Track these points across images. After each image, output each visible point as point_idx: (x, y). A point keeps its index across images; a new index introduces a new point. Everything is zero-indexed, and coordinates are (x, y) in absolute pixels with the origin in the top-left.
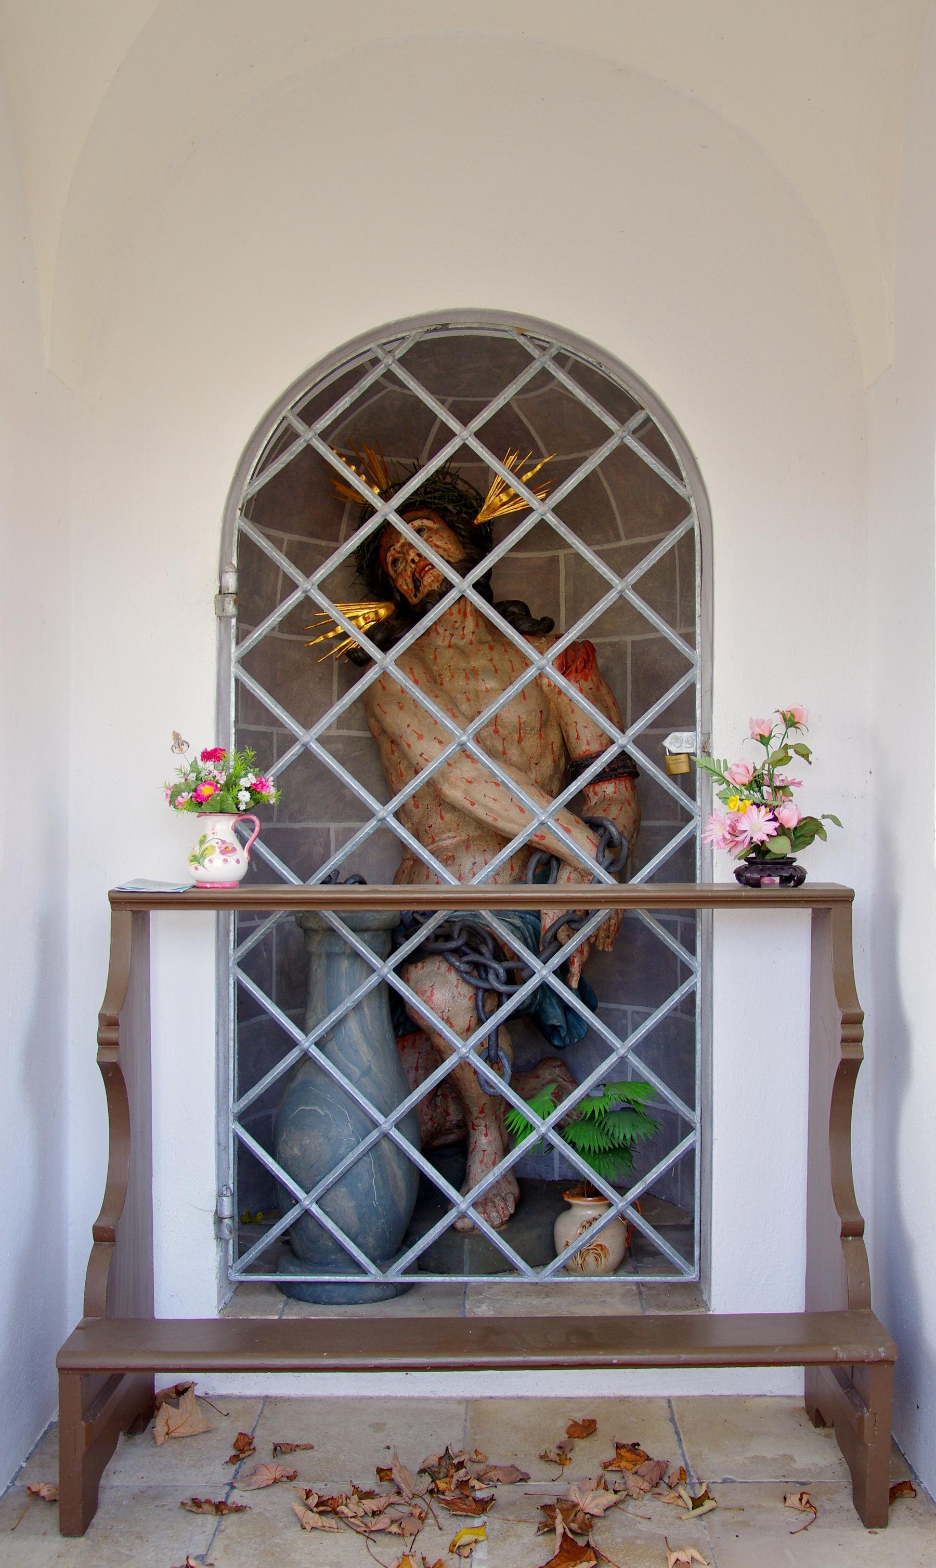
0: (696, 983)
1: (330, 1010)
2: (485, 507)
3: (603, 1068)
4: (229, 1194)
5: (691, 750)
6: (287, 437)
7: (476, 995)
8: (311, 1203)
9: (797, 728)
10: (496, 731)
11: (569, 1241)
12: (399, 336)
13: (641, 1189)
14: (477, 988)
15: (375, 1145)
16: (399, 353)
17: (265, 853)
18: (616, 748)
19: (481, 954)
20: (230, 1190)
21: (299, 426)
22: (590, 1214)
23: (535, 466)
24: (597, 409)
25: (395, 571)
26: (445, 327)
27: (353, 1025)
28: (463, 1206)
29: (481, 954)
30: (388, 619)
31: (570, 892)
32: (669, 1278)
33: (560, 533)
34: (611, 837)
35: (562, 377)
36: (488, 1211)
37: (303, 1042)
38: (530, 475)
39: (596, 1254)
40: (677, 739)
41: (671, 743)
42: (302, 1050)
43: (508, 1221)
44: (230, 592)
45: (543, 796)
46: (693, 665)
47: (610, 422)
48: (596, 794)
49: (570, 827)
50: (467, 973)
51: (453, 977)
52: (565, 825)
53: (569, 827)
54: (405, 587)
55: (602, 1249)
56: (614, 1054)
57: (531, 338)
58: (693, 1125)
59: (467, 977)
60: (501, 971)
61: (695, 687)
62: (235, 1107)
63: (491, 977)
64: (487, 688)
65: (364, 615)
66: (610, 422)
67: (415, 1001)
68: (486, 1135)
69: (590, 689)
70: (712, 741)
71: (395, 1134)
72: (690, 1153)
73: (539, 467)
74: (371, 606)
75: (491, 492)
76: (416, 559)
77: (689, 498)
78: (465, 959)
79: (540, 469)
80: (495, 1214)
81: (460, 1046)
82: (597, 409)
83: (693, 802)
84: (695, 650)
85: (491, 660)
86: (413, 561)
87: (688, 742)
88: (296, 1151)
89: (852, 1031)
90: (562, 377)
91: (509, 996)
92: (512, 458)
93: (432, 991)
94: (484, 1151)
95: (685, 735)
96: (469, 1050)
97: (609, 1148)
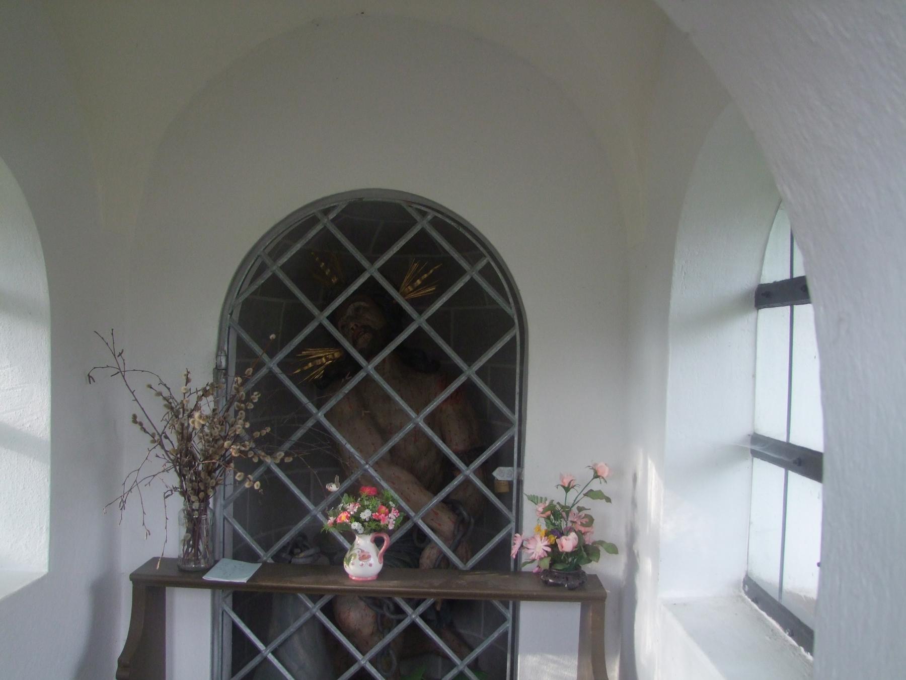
1: (282, 631)
5: (510, 479)
6: (262, 268)
9: (573, 487)
16: (331, 216)
21: (268, 261)
27: (296, 639)
30: (338, 359)
34: (464, 519)
37: (263, 652)
38: (426, 276)
47: (464, 264)
49: (438, 512)
63: (385, 608)
65: (325, 356)
74: (330, 350)
75: (403, 284)
76: (355, 328)
81: (360, 659)
82: (456, 255)
83: (510, 513)
86: (352, 328)
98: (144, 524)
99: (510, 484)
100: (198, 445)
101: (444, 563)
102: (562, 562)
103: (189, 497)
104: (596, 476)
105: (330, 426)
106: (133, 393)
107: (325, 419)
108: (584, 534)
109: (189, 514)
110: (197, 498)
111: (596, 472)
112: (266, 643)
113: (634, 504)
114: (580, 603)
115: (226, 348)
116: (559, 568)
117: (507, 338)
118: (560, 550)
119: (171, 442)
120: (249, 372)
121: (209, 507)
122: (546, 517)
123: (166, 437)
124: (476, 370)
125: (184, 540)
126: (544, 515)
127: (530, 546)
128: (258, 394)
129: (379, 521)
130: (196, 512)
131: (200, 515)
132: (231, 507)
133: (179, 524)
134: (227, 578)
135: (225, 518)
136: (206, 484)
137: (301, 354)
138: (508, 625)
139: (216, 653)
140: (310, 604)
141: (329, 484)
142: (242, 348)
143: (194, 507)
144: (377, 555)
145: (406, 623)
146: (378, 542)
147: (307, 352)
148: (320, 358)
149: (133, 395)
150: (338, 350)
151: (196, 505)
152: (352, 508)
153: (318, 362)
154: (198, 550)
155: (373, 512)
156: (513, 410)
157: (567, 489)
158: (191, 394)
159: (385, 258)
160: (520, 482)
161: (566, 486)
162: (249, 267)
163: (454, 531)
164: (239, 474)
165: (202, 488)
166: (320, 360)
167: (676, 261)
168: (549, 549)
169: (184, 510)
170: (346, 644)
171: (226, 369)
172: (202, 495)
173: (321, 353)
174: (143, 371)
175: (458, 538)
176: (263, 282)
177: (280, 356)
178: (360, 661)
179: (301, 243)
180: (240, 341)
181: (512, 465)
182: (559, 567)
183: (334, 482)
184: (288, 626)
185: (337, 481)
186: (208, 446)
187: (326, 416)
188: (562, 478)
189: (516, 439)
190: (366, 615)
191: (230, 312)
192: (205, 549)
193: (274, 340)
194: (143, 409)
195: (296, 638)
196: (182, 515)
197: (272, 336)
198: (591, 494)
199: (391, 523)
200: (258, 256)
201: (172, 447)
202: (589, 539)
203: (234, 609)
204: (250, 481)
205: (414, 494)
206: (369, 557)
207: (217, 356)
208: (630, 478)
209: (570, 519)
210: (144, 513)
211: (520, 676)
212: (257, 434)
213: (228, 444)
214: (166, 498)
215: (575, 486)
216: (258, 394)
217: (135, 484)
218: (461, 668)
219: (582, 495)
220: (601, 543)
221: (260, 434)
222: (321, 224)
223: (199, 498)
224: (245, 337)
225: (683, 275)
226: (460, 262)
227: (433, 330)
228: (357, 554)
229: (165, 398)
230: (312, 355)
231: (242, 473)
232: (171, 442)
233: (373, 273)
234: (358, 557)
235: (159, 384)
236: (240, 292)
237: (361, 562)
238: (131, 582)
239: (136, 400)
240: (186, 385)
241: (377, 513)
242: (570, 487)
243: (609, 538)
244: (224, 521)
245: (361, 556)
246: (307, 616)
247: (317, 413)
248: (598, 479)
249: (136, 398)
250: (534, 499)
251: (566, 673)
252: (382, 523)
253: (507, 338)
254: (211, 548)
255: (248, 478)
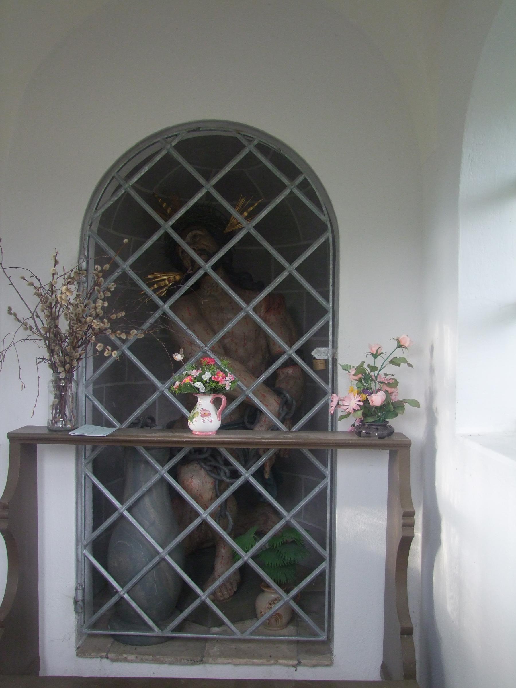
0: (327, 483)
1: (135, 491)
2: (229, 225)
3: (278, 527)
4: (81, 589)
5: (326, 358)
7: (215, 482)
8: (124, 594)
9: (379, 355)
10: (232, 340)
11: (262, 610)
12: (174, 134)
13: (297, 591)
14: (215, 479)
15: (158, 563)
17: (100, 408)
18: (286, 356)
19: (218, 462)
20: (82, 586)
22: (274, 597)
23: (254, 204)
24: (278, 173)
25: (183, 257)
26: (198, 129)
28: (203, 598)
29: (218, 462)
31: (256, 439)
32: (311, 638)
33: (257, 239)
35: (260, 156)
36: (222, 591)
37: (120, 509)
38: (251, 208)
39: (276, 618)
40: (319, 351)
41: (316, 354)
42: (119, 513)
43: (233, 596)
44: (82, 269)
45: (251, 377)
46: (328, 312)
47: (285, 180)
48: (283, 374)
50: (210, 471)
51: (203, 472)
52: (263, 393)
53: (265, 394)
54: (187, 265)
55: (279, 616)
56: (283, 520)
57: (244, 135)
58: (325, 558)
59: (210, 473)
60: (227, 471)
61: (329, 323)
62: (91, 536)
63: (222, 474)
64: (228, 318)
65: (168, 279)
66: (285, 180)
67: (178, 489)
68: (224, 548)
69: (281, 319)
70: (338, 352)
71: (168, 558)
72: (322, 574)
73: (256, 204)
74: (172, 274)
77: (327, 222)
78: (209, 463)
79: (257, 206)
80: (226, 592)
81: (202, 513)
82: (278, 173)
83: (327, 386)
84: (329, 303)
85: (230, 303)
87: (325, 353)
88: (116, 564)
89: (408, 521)
90: (260, 156)
91: (232, 484)
92: (243, 199)
93: (192, 480)
94: (223, 557)
95: (323, 349)
96: (207, 516)
97: (282, 565)
98: (20, 378)
99: (326, 361)
100: (64, 326)
101: (274, 428)
102: (372, 415)
103: (56, 368)
104: (400, 346)
105: (174, 316)
106: (9, 278)
107: (170, 310)
108: (391, 393)
109: (57, 381)
110: (63, 369)
111: (399, 342)
112: (122, 503)
113: (432, 370)
114: (388, 451)
115: (86, 254)
116: (370, 421)
117: (322, 240)
118: (371, 404)
119: (42, 321)
120: (106, 267)
121: (73, 379)
122: (358, 379)
123: (38, 316)
124: (296, 267)
125: (53, 405)
126: (356, 378)
127: (345, 403)
128: (114, 285)
129: (218, 382)
130: (63, 381)
131: (66, 383)
132: (91, 387)
133: (49, 392)
134: (90, 434)
135: (86, 397)
136: (71, 357)
137: (148, 277)
138: (328, 481)
139: (79, 513)
140: (158, 467)
141: (175, 354)
142: (99, 252)
143: (61, 377)
144: (216, 414)
145: (239, 482)
146: (217, 403)
147: (153, 276)
148: (164, 280)
149: (10, 280)
150: (178, 274)
151: (63, 376)
152: (195, 373)
153: (162, 284)
154: (65, 414)
155: (212, 375)
156: (328, 300)
157: (375, 356)
158: (58, 277)
159: (219, 176)
160: (335, 361)
161: (374, 353)
162: (106, 186)
163: (279, 410)
164: (99, 345)
165: (68, 361)
166: (163, 282)
167: (464, 150)
168: (361, 404)
169: (52, 381)
170: (189, 500)
171: (87, 270)
172: (68, 366)
173: (164, 276)
174: (17, 268)
175: (283, 415)
176: (117, 198)
177: (132, 259)
178: (201, 514)
179: (149, 165)
180: (98, 247)
181: (327, 346)
182: (370, 420)
183: (179, 353)
184: (141, 487)
185: (181, 352)
186: (73, 323)
187: (171, 307)
188: (370, 347)
189: (331, 323)
190: (206, 481)
191: (90, 223)
192: (70, 414)
193: (126, 243)
194: (18, 292)
195: (147, 500)
196: (51, 385)
197: (126, 241)
198: (395, 362)
199: (227, 384)
200: (113, 178)
201: (43, 326)
202: (395, 398)
203: (95, 473)
204: (109, 350)
205: (245, 380)
206: (210, 414)
207: (79, 259)
208: (427, 352)
209: (378, 380)
210: (20, 368)
211: (338, 525)
212: (114, 317)
213: (90, 319)
214: (38, 363)
215: (382, 353)
216: (114, 285)
217: (13, 343)
218: (288, 518)
219: (387, 362)
220: (406, 401)
221: (117, 317)
222: (165, 150)
223: (65, 369)
224: (102, 244)
225: (470, 161)
226: (281, 179)
227: (260, 235)
228: (200, 412)
229: (35, 288)
230: (157, 278)
231: (102, 344)
232: (42, 321)
233: (209, 189)
234: (200, 414)
235: (31, 277)
236: (98, 208)
237: (203, 418)
238: (8, 440)
239: (12, 284)
240: (55, 267)
241: (216, 376)
242: (378, 354)
243: (413, 397)
244: (85, 559)
245: (203, 413)
246: (157, 477)
247: (163, 306)
248: (401, 348)
249: (12, 283)
250: (346, 368)
251: (377, 522)
252: (220, 384)
253: (322, 240)
254: (75, 414)
255: (107, 349)
